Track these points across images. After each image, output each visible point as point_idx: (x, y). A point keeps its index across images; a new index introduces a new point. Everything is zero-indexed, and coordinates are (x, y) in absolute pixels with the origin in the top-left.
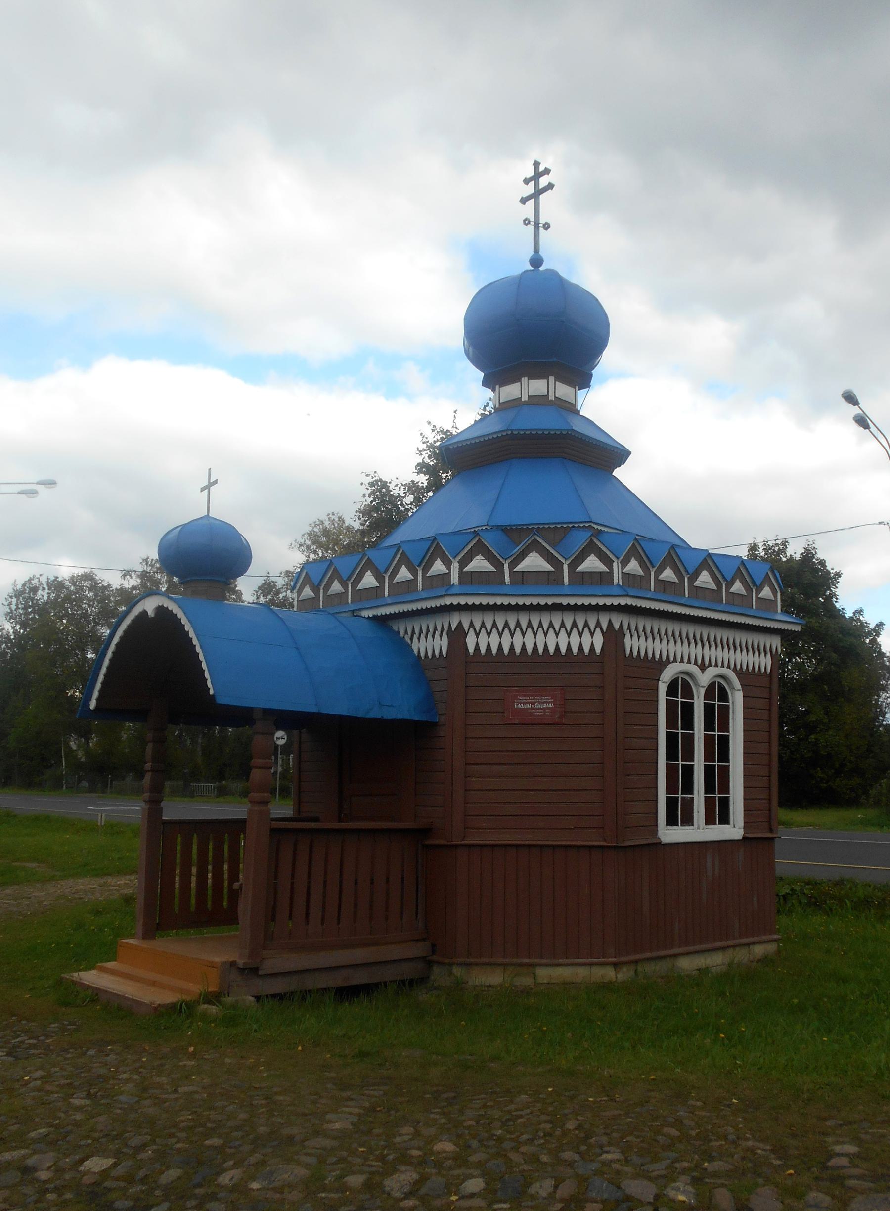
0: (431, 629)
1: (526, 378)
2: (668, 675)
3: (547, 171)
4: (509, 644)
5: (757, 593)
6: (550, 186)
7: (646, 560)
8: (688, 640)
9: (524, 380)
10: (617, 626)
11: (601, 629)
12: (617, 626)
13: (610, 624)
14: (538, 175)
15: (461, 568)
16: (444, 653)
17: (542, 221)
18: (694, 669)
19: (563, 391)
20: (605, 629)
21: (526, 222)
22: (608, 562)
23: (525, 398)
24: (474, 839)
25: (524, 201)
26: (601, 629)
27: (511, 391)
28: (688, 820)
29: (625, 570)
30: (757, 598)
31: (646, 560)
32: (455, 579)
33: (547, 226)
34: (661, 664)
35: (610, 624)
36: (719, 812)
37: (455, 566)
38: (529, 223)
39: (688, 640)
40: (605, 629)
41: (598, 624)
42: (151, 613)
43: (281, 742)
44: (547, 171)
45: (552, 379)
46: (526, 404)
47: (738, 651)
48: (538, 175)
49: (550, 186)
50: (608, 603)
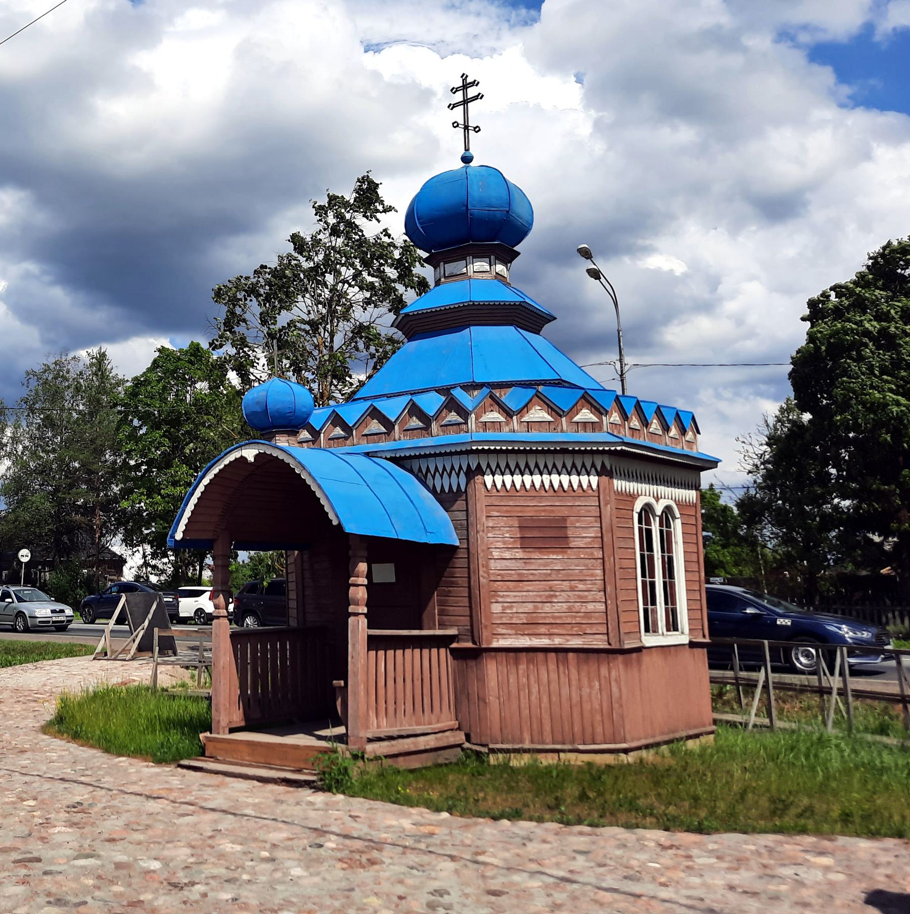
2: (638, 506)
3: (474, 83)
4: (530, 482)
6: (479, 97)
11: (596, 469)
14: (465, 86)
15: (477, 419)
17: (472, 124)
18: (653, 501)
20: (599, 468)
21: (477, 129)
24: (495, 645)
25: (452, 106)
28: (655, 631)
33: (477, 129)
34: (633, 497)
36: (673, 625)
38: (458, 126)
42: (251, 459)
43: (25, 560)
44: (474, 83)
48: (465, 86)
49: (479, 97)
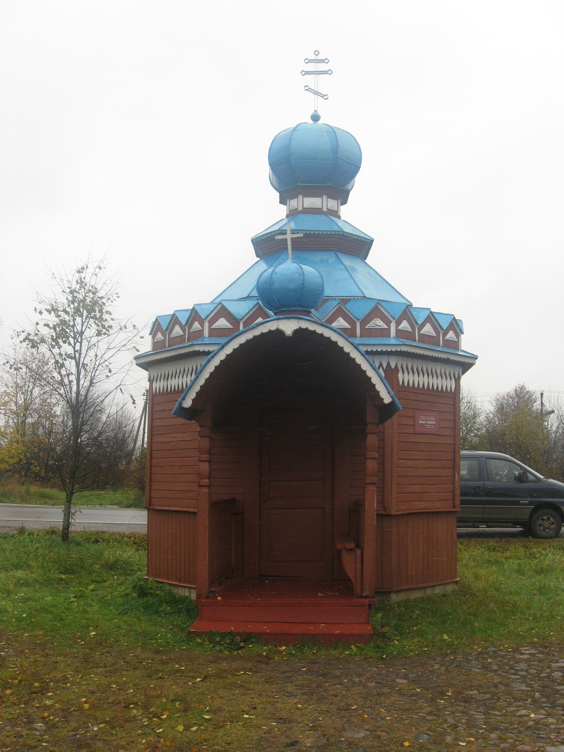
0: (178, 372)
1: (301, 196)
5: (420, 330)
7: (437, 325)
8: (408, 370)
9: (300, 197)
10: (393, 366)
11: (383, 368)
12: (393, 366)
13: (389, 365)
16: (453, 390)
19: (332, 204)
20: (385, 367)
22: (388, 323)
23: (300, 209)
26: (383, 368)
27: (294, 203)
29: (400, 328)
30: (419, 334)
31: (437, 325)
32: (206, 333)
35: (389, 365)
37: (206, 325)
39: (408, 370)
40: (385, 367)
41: (381, 365)
45: (325, 197)
46: (301, 212)
47: (421, 375)
50: (394, 350)
